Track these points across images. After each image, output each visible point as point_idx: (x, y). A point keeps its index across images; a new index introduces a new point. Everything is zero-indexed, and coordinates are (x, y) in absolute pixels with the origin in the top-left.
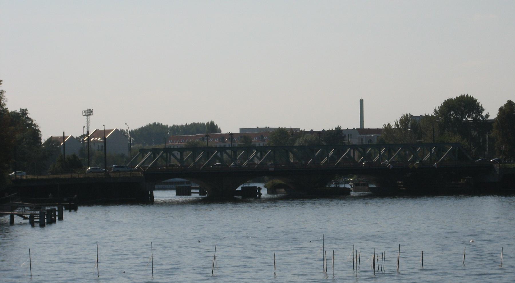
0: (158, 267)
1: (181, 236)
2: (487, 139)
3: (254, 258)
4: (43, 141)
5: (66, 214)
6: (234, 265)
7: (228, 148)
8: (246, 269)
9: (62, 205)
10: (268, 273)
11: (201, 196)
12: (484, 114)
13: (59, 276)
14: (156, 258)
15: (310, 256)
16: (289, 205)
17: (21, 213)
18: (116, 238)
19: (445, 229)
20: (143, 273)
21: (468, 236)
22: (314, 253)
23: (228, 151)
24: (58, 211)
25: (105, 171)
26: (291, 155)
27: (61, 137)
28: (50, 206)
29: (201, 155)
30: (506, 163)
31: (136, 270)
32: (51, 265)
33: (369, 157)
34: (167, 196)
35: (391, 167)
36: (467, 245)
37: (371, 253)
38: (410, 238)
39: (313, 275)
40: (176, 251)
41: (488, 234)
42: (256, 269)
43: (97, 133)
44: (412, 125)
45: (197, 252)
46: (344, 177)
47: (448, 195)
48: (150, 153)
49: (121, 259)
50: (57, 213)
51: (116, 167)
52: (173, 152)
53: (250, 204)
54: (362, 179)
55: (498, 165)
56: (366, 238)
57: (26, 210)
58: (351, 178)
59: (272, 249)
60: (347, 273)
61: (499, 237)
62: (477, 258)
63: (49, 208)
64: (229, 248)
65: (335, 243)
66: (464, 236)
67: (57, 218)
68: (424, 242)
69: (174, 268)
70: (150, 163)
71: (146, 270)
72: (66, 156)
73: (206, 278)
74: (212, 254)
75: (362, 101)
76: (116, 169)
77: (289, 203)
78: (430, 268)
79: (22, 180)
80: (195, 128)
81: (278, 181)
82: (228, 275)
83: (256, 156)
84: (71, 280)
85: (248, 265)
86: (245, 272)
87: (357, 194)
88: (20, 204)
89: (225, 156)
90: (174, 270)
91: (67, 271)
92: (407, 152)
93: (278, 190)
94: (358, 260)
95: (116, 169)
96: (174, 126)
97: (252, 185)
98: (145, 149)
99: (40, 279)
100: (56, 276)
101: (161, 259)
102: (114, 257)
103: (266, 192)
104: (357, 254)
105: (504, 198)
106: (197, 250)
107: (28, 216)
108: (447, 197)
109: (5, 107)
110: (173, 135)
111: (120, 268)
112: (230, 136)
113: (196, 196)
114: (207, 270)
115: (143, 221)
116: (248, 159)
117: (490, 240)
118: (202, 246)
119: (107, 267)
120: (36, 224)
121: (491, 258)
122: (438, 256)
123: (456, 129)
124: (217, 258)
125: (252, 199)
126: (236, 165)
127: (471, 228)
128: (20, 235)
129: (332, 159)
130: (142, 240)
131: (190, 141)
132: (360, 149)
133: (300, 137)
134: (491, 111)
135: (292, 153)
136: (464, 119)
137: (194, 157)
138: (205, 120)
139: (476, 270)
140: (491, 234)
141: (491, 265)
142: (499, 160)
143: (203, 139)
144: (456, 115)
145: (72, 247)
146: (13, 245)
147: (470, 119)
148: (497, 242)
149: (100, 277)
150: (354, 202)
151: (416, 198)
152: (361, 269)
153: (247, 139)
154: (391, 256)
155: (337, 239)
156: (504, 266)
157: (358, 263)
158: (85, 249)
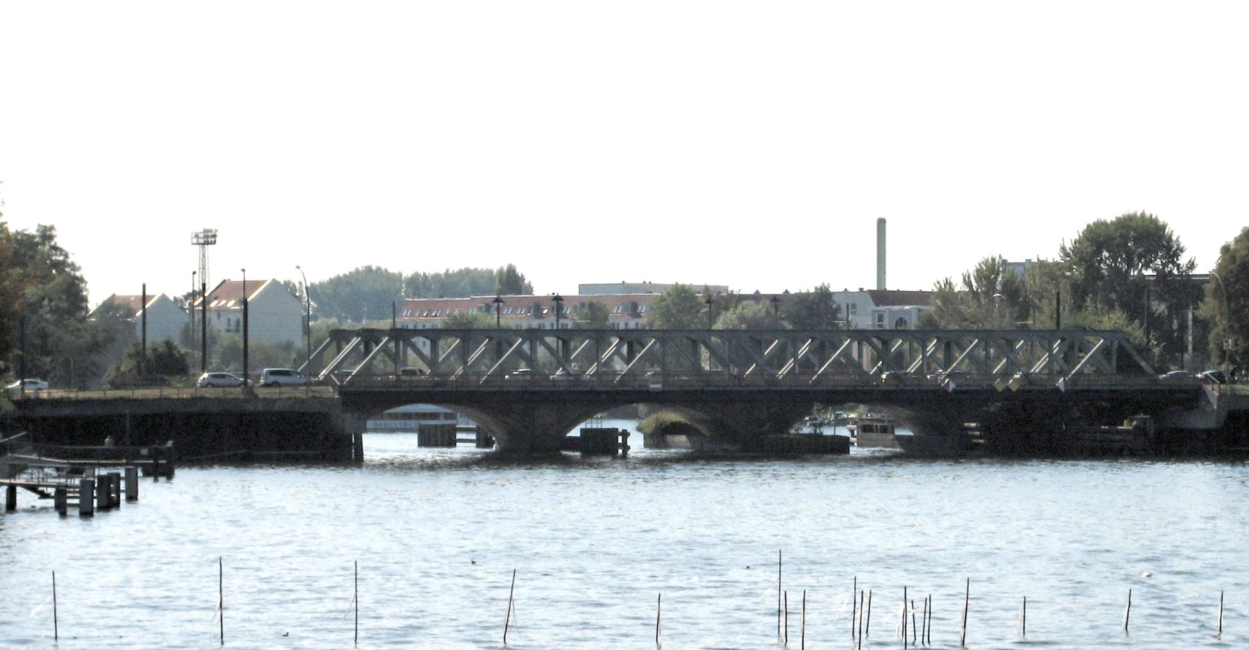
0: (371, 624)
2: (1190, 323)
4: (92, 306)
5: (146, 486)
8: (589, 633)
9: (137, 465)
12: (1183, 260)
13: (123, 640)
14: (365, 601)
15: (748, 603)
16: (697, 475)
17: (35, 482)
19: (1081, 542)
20: (332, 636)
21: (1140, 560)
22: (757, 595)
25: (245, 383)
26: (704, 353)
27: (136, 297)
30: (1234, 382)
31: (316, 630)
32: (105, 611)
33: (899, 361)
35: (952, 386)
36: (1135, 583)
38: (995, 564)
41: (1189, 558)
42: (612, 632)
44: (1004, 285)
45: (467, 587)
46: (834, 411)
48: (355, 340)
49: (279, 603)
50: (123, 485)
51: (272, 373)
52: (414, 340)
53: (601, 472)
54: (878, 416)
56: (886, 561)
58: (852, 410)
59: (653, 584)
61: (1215, 566)
62: (1160, 616)
63: (103, 472)
64: (547, 578)
65: (810, 572)
66: (1129, 561)
67: (123, 496)
68: (1030, 574)
69: (411, 627)
71: (340, 630)
72: (148, 345)
75: (881, 223)
76: (272, 379)
77: (697, 470)
78: (1043, 639)
79: (40, 402)
80: (467, 282)
83: (618, 352)
85: (593, 621)
86: (586, 640)
87: (865, 452)
88: (31, 460)
89: (541, 351)
90: (411, 630)
91: (144, 629)
93: (669, 438)
94: (865, 615)
98: (344, 331)
100: (117, 641)
101: (377, 602)
103: (642, 442)
104: (862, 601)
106: (469, 582)
107: (52, 491)
108: (1088, 463)
111: (275, 624)
112: (554, 303)
113: (468, 450)
115: (337, 507)
116: (597, 358)
117: (1192, 573)
118: (479, 574)
119: (244, 620)
120: (70, 511)
121: (1193, 617)
122: (1063, 610)
125: (606, 460)
127: (1147, 542)
128: (31, 538)
129: (806, 365)
130: (331, 555)
132: (875, 340)
133: (727, 309)
134: (1202, 254)
135: (708, 347)
136: (1133, 273)
137: (464, 352)
138: (492, 261)
140: (1194, 558)
141: (1193, 635)
142: (1220, 377)
144: (1115, 261)
145: (158, 570)
147: (1149, 272)
148: (1209, 578)
149: (227, 645)
150: (857, 470)
152: (873, 638)
154: (948, 609)
155: (814, 563)
156: (1225, 638)
157: (864, 622)
158: (191, 575)
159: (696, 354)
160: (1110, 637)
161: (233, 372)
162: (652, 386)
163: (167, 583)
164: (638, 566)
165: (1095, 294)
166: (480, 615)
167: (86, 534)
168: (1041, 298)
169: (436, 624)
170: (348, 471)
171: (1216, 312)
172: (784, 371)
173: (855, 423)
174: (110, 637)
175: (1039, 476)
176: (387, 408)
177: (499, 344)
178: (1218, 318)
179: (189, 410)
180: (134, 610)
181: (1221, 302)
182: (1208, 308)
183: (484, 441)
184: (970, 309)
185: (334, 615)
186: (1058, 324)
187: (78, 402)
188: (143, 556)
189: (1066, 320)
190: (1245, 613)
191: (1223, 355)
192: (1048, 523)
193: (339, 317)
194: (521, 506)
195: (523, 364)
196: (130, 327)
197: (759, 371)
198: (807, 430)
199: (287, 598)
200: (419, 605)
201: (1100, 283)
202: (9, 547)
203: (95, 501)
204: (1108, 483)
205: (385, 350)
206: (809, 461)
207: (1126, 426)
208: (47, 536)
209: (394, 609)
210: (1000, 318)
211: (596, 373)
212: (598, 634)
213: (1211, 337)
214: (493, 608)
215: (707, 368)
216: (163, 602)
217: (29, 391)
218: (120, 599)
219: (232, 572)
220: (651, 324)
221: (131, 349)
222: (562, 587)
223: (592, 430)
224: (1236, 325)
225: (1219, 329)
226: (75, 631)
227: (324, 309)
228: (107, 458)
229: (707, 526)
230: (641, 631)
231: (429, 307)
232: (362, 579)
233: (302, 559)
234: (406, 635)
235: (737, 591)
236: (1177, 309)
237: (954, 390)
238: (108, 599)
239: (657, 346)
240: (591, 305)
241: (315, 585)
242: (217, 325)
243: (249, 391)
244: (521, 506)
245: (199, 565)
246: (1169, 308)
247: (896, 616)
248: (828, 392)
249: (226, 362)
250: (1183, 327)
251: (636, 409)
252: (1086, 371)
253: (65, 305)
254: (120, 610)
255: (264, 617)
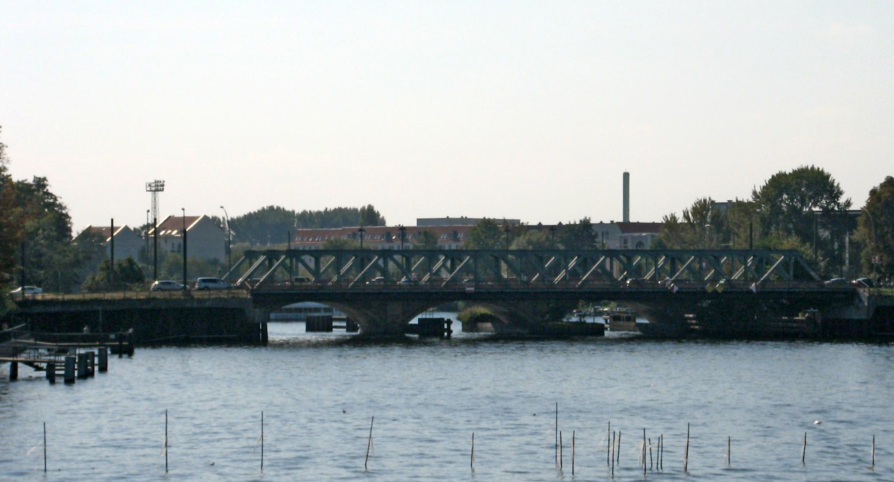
0: (273, 455)
1: (314, 401)
2: (847, 245)
3: (438, 441)
4: (74, 235)
5: (114, 362)
6: (402, 452)
7: (397, 252)
8: (424, 461)
9: (107, 346)
10: (461, 469)
11: (348, 334)
12: (842, 200)
13: (95, 471)
14: (268, 439)
15: (535, 439)
16: (499, 350)
17: (32, 359)
18: (200, 404)
19: (769, 399)
20: (245, 465)
21: (812, 412)
22: (541, 434)
23: (396, 257)
24: (100, 356)
25: (185, 288)
26: (504, 266)
27: (107, 228)
28: (84, 347)
29: (350, 263)
30: (881, 286)
31: (234, 461)
32: (82, 450)
33: (638, 271)
34: (290, 332)
35: (676, 289)
36: (809, 428)
37: (640, 438)
38: (707, 414)
39: (539, 473)
40: (305, 427)
41: (848, 411)
42: (440, 460)
43: (171, 222)
44: (713, 218)
45: (340, 429)
46: (594, 306)
47: (776, 341)
48: (262, 258)
49: (208, 442)
50: (96, 360)
51: (204, 281)
52: (303, 257)
53: (433, 348)
54: (624, 310)
55: (866, 290)
56: (630, 411)
57: (41, 354)
58: (606, 305)
59: (469, 426)
60: (597, 471)
61: (867, 417)
62: (828, 452)
63: (82, 351)
64: (395, 422)
65: (577, 418)
66: (804, 413)
67: (96, 368)
68: (732, 420)
69: (300, 457)
70: (262, 274)
71: (250, 460)
72: (115, 261)
73: (354, 475)
74: (366, 434)
75: (626, 176)
76: (203, 285)
77: (498, 347)
78: (743, 467)
79: (36, 302)
80: (341, 216)
81: (481, 310)
82: (392, 471)
83: (444, 265)
84: (118, 478)
85: (427, 452)
86: (422, 466)
87: (616, 334)
88: (29, 344)
89: (391, 265)
90: (301, 460)
91: (111, 462)
92: (704, 264)
93: (480, 325)
94: (616, 449)
95: (203, 285)
96: (304, 213)
97: (437, 315)
98: (254, 252)
99: (61, 477)
100: (90, 471)
101: (277, 440)
102: (195, 437)
103: (461, 328)
104: (614, 438)
105: (876, 347)
106: (342, 425)
107: (44, 365)
108: (774, 343)
109: (5, 174)
110: (303, 227)
111: (205, 457)
112: (400, 232)
113: (340, 333)
114: (356, 460)
115: (249, 374)
116: (430, 270)
117: (851, 422)
118: (348, 420)
119: (183, 455)
120: (57, 380)
121: (853, 454)
122: (756, 447)
123: (791, 226)
124: (374, 441)
125: (436, 340)
126: (409, 281)
127: (817, 400)
128: (28, 399)
129: (574, 274)
130: (245, 407)
131: (332, 238)
132: (622, 257)
133: (519, 235)
134: (856, 194)
135: (506, 262)
136: (806, 209)
137: (337, 266)
138: (357, 203)
139: (825, 474)
140: (852, 412)
141: (853, 467)
142: (869, 282)
143: (354, 235)
144: (792, 201)
145: (121, 420)
146: (14, 416)
147: (817, 209)
148: (864, 426)
149: (170, 472)
150: (610, 347)
151: (718, 344)
152: (622, 465)
153: (431, 238)
154: (675, 444)
155: (580, 411)
156: (877, 469)
157: (616, 454)
158: (145, 423)
159: (498, 267)
160: (791, 467)
161: (176, 280)
162: (468, 289)
163: (128, 429)
164: (458, 414)
165: (778, 224)
166: (349, 448)
167: (69, 395)
168: (739, 227)
169: (318, 455)
170: (257, 349)
171: (867, 236)
172: (558, 278)
173: (608, 314)
174: (85, 469)
175: (738, 351)
176: (284, 305)
177: (362, 260)
178: (867, 241)
179: (145, 306)
180: (104, 449)
181: (870, 230)
182: (860, 233)
183: (351, 327)
184: (688, 236)
185: (247, 450)
186: (751, 246)
187: (64, 303)
188: (111, 410)
189: (756, 243)
190: (891, 451)
191: (872, 267)
192: (745, 385)
193: (251, 242)
194: (377, 372)
195: (379, 274)
196: (103, 249)
197: (542, 278)
198: (574, 319)
199: (213, 438)
200: (306, 442)
201: (781, 217)
202: (12, 406)
203: (76, 372)
204: (788, 357)
205: (283, 264)
206: (576, 341)
207: (800, 317)
208: (40, 397)
209: (289, 445)
210: (711, 242)
211: (429, 280)
212: (431, 461)
213: (863, 254)
214: (358, 444)
215: (505, 276)
216: (124, 443)
217: (28, 295)
218: (92, 441)
219: (174, 420)
220: (467, 246)
221: (102, 264)
222: (406, 429)
223: (426, 319)
224: (881, 246)
225: (869, 249)
226: (59, 465)
227: (240, 237)
228: (85, 342)
229: (506, 386)
230: (461, 459)
231: (314, 234)
232: (267, 424)
233: (224, 410)
234: (296, 464)
235: (527, 431)
236: (837, 235)
237: (677, 292)
238: (84, 441)
239: (471, 261)
240: (426, 233)
241: (234, 429)
242: (165, 247)
243: (187, 292)
244: (377, 372)
245: (151, 416)
246: (832, 234)
247: (638, 449)
248: (589, 293)
249: (171, 273)
250: (842, 247)
251: (456, 305)
252: (771, 279)
253: (54, 234)
254: (92, 449)
255: (198, 451)
